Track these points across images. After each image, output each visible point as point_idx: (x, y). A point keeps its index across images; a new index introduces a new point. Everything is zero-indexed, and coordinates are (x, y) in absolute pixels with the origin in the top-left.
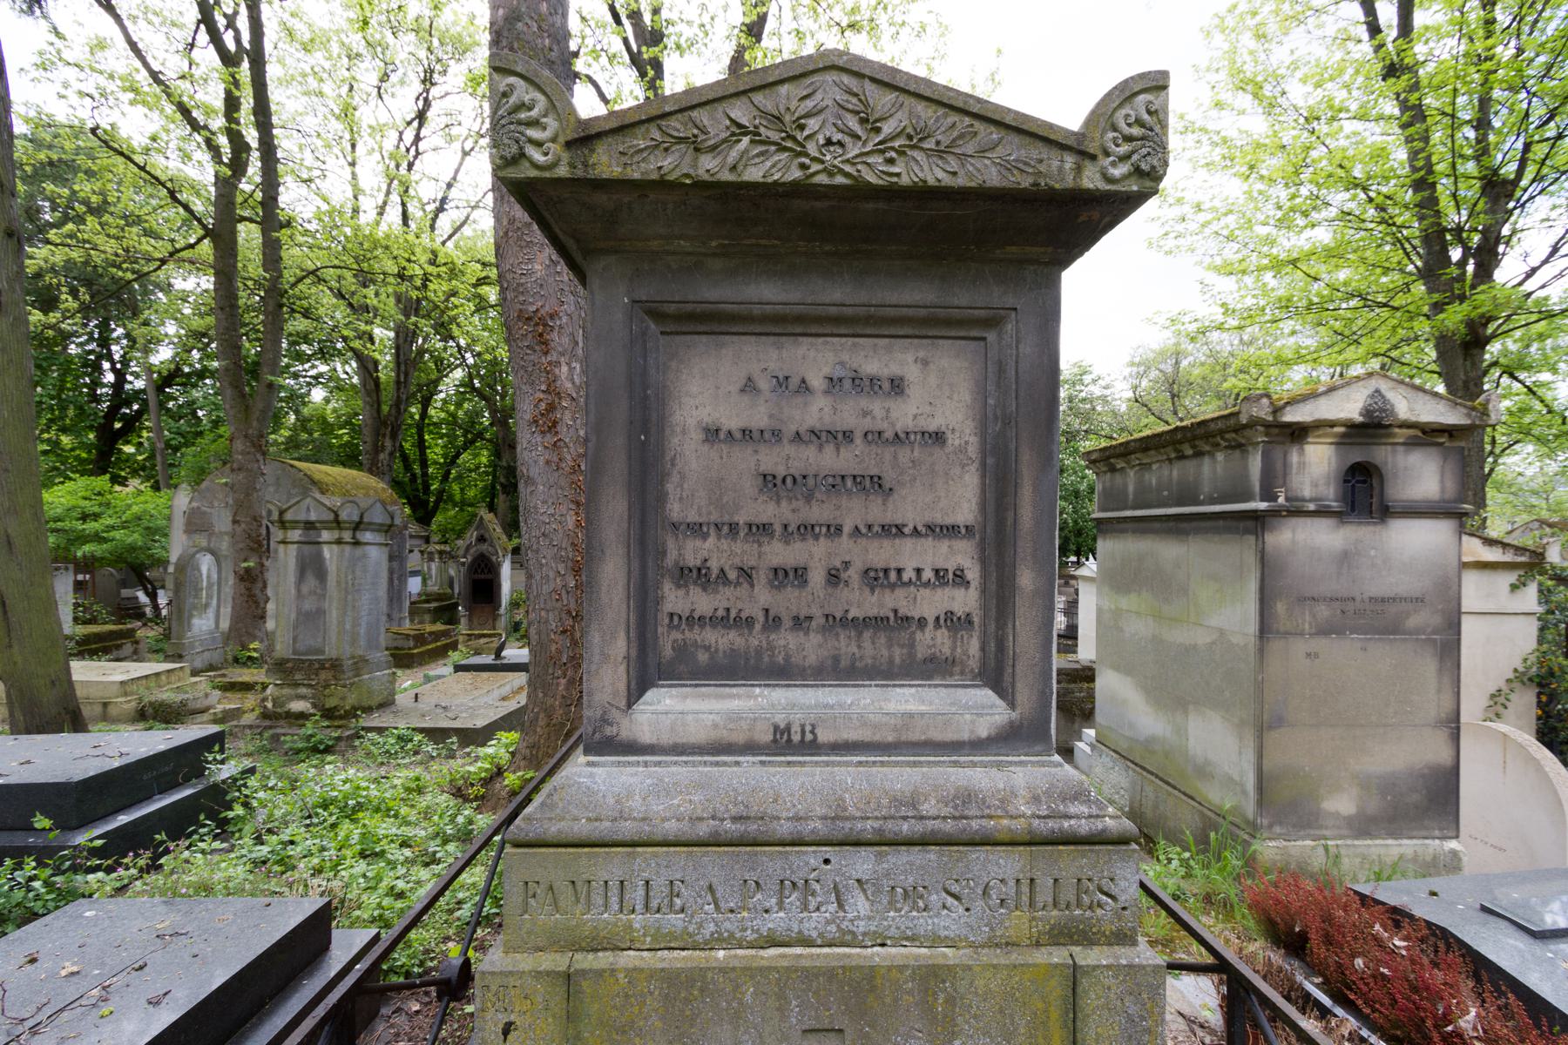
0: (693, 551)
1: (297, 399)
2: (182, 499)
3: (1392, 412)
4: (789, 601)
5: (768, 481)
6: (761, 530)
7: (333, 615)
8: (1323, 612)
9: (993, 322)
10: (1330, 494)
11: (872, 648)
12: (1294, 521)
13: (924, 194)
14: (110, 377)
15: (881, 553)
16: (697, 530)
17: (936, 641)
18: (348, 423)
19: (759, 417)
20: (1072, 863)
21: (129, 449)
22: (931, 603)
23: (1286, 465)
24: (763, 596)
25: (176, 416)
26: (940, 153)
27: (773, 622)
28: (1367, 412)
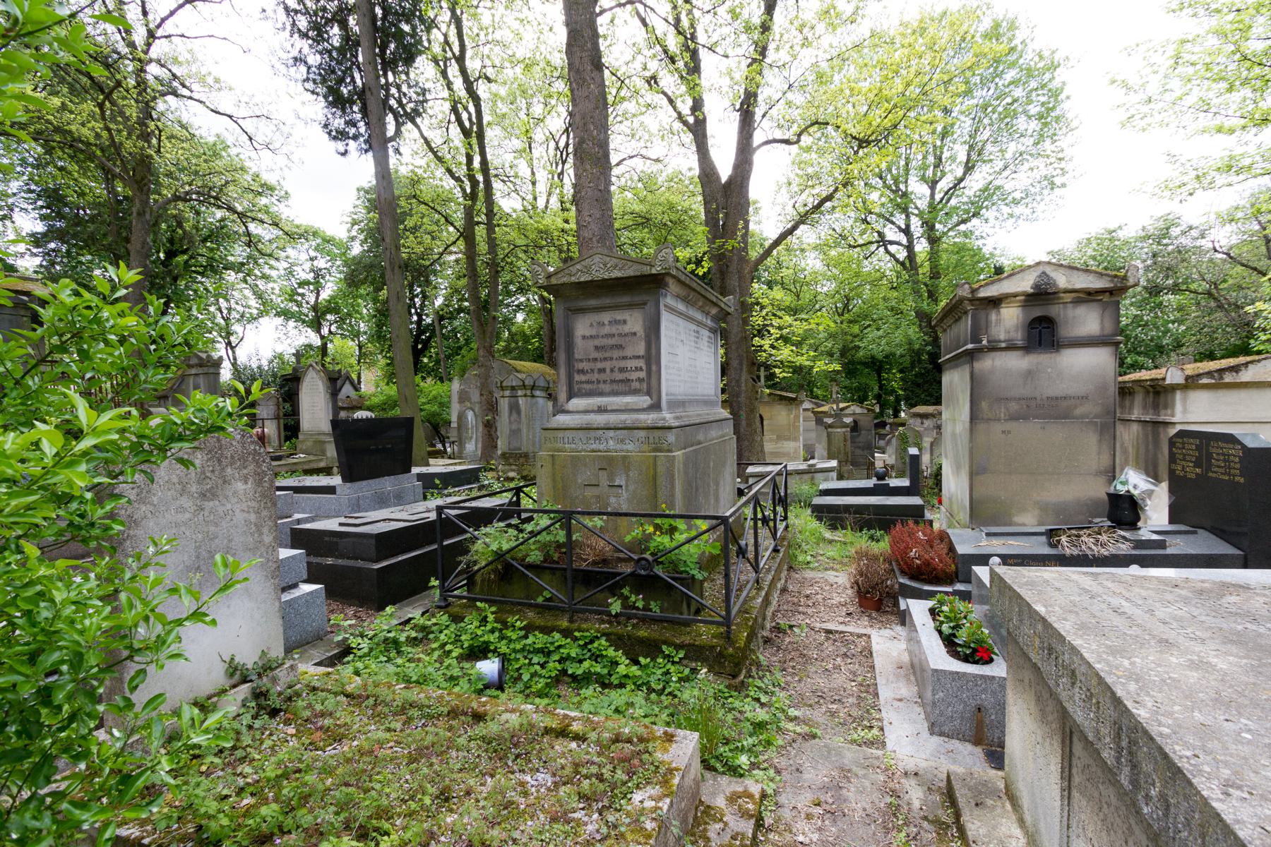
0: (580, 366)
1: (508, 321)
2: (456, 385)
3: (1055, 284)
4: (602, 377)
5: (597, 348)
6: (595, 360)
7: (524, 431)
8: (1014, 406)
9: (645, 304)
10: (1019, 337)
11: (621, 387)
12: (993, 354)
13: (617, 279)
14: (415, 318)
15: (622, 364)
16: (581, 361)
17: (636, 385)
18: (538, 334)
19: (593, 332)
20: (657, 433)
21: (425, 360)
22: (634, 376)
23: (988, 322)
24: (596, 376)
25: (447, 338)
26: (620, 269)
27: (599, 382)
28: (1036, 286)
